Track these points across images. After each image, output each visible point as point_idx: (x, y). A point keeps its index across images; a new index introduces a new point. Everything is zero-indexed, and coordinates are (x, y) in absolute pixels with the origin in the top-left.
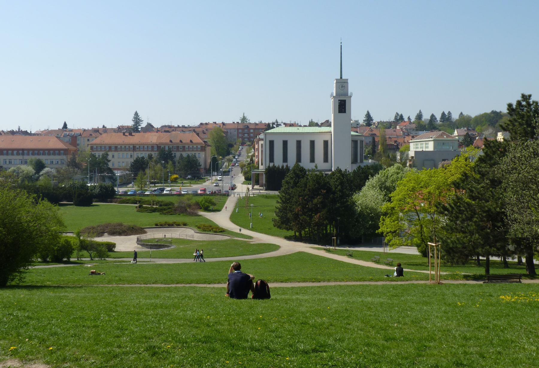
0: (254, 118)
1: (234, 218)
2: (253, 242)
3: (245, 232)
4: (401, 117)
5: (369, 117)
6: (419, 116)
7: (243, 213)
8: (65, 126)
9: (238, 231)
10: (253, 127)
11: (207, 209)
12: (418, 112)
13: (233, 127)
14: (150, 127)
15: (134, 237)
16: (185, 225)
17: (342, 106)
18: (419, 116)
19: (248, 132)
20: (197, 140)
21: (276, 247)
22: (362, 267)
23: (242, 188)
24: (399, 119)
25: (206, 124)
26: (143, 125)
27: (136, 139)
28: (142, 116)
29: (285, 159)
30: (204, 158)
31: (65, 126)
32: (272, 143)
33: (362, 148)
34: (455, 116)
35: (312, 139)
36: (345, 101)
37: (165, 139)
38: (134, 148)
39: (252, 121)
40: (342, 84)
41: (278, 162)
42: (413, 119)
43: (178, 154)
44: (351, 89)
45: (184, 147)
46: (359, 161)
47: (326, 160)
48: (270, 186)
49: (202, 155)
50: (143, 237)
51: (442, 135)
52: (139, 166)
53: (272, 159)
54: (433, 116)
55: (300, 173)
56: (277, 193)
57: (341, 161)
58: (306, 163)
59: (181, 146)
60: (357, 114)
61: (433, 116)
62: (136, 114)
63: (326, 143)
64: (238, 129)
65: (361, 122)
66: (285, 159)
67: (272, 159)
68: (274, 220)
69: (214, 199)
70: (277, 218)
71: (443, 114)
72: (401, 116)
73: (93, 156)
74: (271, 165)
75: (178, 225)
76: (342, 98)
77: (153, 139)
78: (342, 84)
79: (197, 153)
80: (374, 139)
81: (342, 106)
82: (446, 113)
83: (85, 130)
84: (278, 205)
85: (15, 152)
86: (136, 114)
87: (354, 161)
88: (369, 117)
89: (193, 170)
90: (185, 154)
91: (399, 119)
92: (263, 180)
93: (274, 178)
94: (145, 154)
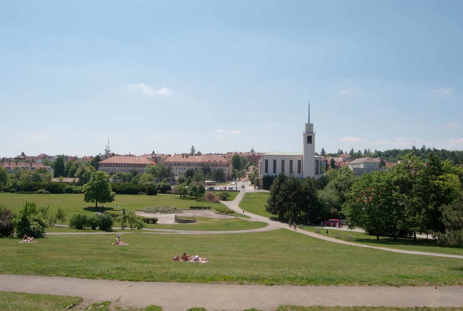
0: (257, 151)
1: (241, 205)
2: (251, 220)
3: (246, 213)
4: (342, 152)
5: (323, 151)
6: (352, 151)
7: (247, 203)
8: (153, 152)
9: (242, 213)
10: (257, 155)
11: (224, 199)
12: (351, 149)
13: (246, 155)
14: (199, 154)
15: (173, 215)
16: (209, 208)
17: (309, 139)
18: (352, 151)
19: (253, 158)
20: (224, 160)
21: (265, 225)
22: (393, 253)
23: (250, 188)
24: (341, 153)
25: (231, 153)
26: (196, 153)
27: (191, 159)
28: (195, 148)
29: (275, 171)
30: (228, 171)
31: (153, 152)
32: (267, 161)
33: (321, 165)
34: (373, 151)
35: (291, 159)
36: (308, 143)
37: (206, 160)
38: (189, 164)
39: (257, 152)
40: (309, 127)
41: (270, 172)
42: (348, 153)
43: (213, 168)
44: (315, 130)
45: (217, 164)
46: (319, 173)
47: (299, 172)
48: (266, 187)
49: (227, 169)
50: (180, 215)
51: (368, 159)
52: (190, 174)
53: (266, 171)
54: (359, 151)
55: (283, 178)
56: (269, 191)
57: (309, 172)
58: (287, 173)
59: (215, 163)
60: (319, 146)
61: (359, 151)
62: (193, 147)
63: (299, 162)
64: (249, 156)
65: (319, 153)
66: (275, 171)
67: (266, 171)
68: (266, 206)
69: (230, 193)
70: (268, 205)
71: (366, 150)
72: (342, 151)
73: (164, 168)
74: (266, 174)
75: (205, 208)
76: (310, 135)
77: (199, 160)
78: (309, 127)
79: (224, 168)
80: (327, 163)
81: (309, 139)
82: (367, 150)
83: (163, 155)
84: (270, 196)
85: (124, 165)
86: (193, 147)
87: (317, 173)
88: (323, 151)
89: (220, 178)
90: (217, 168)
91: (341, 153)
92: (261, 183)
93: (267, 183)
94: (194, 168)
